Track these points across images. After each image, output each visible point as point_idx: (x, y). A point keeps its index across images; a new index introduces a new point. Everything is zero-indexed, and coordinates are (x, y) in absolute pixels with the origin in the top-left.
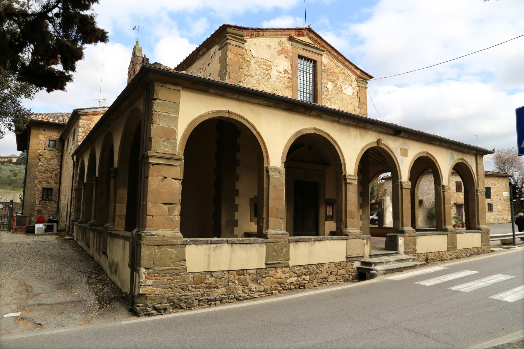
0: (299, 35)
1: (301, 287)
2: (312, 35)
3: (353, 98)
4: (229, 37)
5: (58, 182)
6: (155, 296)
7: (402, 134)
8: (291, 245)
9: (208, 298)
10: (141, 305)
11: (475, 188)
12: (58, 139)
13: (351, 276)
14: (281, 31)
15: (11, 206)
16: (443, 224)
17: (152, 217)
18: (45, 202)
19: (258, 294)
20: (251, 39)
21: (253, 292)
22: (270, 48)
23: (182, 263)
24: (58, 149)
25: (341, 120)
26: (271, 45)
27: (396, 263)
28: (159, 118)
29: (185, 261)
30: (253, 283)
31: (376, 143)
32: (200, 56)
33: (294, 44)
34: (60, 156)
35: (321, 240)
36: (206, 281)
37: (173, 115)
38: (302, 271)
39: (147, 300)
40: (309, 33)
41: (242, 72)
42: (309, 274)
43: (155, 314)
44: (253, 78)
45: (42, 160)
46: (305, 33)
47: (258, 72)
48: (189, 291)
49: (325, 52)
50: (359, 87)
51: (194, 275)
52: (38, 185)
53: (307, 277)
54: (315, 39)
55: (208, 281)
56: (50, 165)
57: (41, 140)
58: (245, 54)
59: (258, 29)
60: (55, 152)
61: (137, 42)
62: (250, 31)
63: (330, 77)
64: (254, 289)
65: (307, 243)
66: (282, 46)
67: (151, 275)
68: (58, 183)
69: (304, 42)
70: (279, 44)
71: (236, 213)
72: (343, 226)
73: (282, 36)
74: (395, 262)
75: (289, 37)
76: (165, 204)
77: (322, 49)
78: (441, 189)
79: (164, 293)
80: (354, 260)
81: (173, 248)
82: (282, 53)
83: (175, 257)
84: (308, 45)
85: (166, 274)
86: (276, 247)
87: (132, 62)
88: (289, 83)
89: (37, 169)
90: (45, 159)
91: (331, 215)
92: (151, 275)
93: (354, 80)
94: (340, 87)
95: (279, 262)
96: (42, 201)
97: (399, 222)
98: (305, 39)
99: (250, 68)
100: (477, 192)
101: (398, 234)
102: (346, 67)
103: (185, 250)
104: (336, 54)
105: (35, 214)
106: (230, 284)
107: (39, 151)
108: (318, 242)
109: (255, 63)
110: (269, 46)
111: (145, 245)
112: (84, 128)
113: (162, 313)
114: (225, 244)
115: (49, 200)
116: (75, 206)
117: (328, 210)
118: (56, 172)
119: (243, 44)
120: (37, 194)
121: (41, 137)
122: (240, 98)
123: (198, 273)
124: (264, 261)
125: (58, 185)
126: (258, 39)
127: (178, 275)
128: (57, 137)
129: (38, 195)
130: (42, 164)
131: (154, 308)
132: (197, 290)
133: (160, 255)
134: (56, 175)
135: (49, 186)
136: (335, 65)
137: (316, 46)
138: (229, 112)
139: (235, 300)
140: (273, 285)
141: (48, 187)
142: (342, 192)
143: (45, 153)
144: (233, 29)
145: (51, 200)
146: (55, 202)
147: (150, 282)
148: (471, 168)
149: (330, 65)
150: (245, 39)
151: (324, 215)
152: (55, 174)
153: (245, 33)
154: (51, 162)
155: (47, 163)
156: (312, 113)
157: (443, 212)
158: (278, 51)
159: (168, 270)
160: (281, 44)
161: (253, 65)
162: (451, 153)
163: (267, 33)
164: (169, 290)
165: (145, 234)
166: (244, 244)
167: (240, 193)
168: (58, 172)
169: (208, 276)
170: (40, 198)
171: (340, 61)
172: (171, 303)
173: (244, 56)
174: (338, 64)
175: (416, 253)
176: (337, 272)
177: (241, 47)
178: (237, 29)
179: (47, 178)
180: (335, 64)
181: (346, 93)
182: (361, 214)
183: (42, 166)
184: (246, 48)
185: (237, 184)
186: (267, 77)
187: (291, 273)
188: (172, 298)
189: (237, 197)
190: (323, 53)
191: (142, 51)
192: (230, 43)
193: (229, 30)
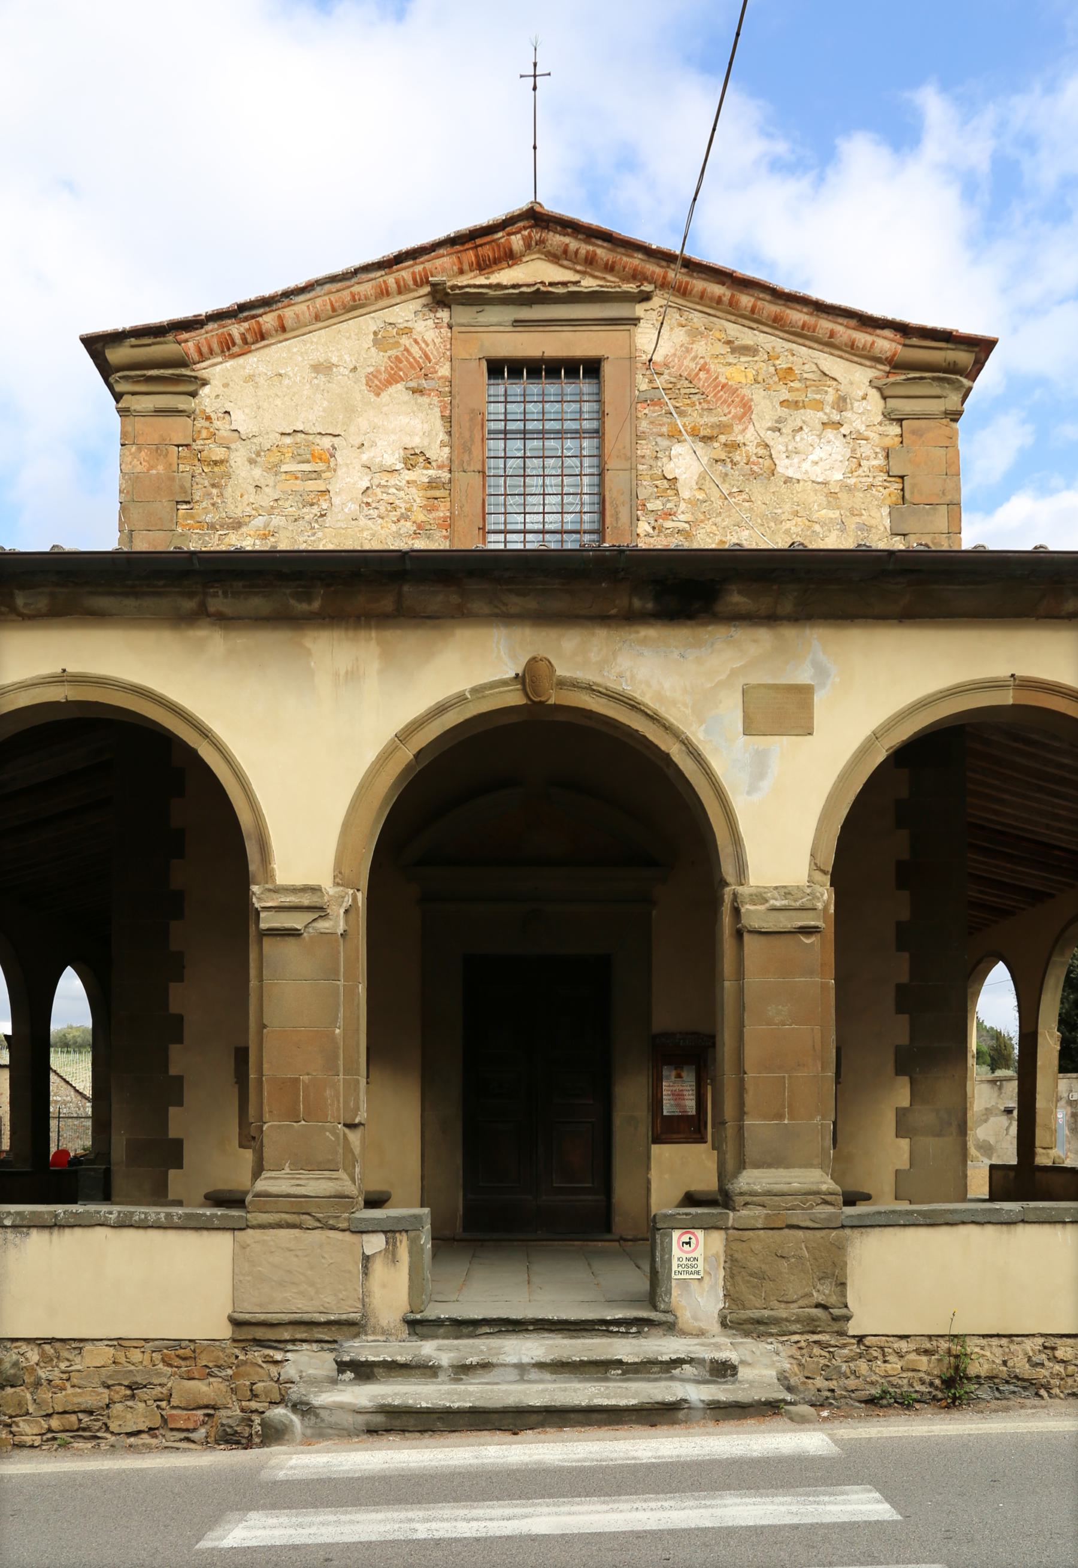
0: (483, 266)
2: (556, 240)
3: (849, 489)
14: (372, 275)
20: (230, 364)
26: (334, 360)
27: (548, 1376)
40: (536, 235)
41: (192, 517)
44: (244, 529)
46: (517, 242)
47: (265, 500)
49: (657, 301)
50: (900, 421)
54: (583, 252)
58: (204, 434)
59: (242, 307)
62: (210, 326)
69: (514, 286)
71: (173, 1111)
73: (393, 301)
74: (534, 1374)
77: (630, 287)
82: (393, 379)
84: (539, 296)
88: (430, 509)
91: (692, 1112)
94: (762, 451)
99: (228, 492)
102: (802, 335)
104: (717, 290)
109: (252, 462)
117: (667, 1087)
119: (193, 394)
126: (266, 350)
137: (589, 284)
142: (248, 981)
144: (133, 346)
149: (694, 358)
151: (643, 1114)
153: (190, 343)
158: (370, 379)
161: (243, 474)
163: (300, 308)
167: (189, 1031)
171: (752, 318)
174: (747, 336)
175: (842, 1333)
181: (798, 476)
182: (905, 1103)
184: (208, 410)
185: (175, 990)
186: (315, 510)
189: (178, 1046)
190: (639, 310)
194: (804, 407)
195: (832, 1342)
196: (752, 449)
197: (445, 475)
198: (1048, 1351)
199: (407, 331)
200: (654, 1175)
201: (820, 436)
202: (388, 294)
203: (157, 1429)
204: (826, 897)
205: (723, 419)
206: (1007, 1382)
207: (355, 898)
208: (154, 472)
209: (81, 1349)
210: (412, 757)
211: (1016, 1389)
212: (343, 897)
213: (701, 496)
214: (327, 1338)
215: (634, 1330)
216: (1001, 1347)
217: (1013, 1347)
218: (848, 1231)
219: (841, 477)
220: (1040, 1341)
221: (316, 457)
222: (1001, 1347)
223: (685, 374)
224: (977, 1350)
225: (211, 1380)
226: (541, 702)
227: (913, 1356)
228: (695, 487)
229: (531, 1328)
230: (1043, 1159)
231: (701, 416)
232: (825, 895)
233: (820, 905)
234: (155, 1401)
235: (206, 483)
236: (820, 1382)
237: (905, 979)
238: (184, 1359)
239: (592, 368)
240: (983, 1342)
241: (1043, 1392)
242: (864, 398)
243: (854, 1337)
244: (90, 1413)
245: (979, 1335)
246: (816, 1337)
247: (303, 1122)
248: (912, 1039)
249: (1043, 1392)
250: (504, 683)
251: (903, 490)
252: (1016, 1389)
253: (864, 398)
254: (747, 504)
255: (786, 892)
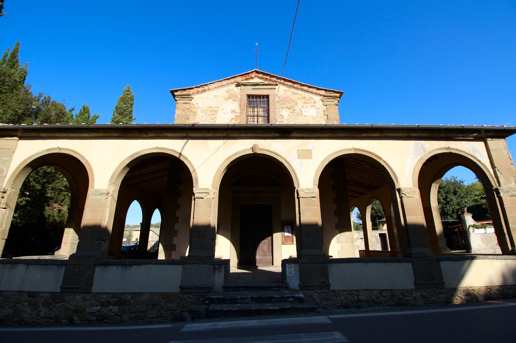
1: (101, 319)
8: (98, 270)
19: (45, 320)
26: (219, 95)
38: (109, 300)
40: (257, 74)
58: (192, 107)
64: (42, 314)
65: (120, 267)
69: (252, 83)
73: (230, 85)
77: (274, 83)
80: (194, 291)
82: (229, 98)
84: (257, 85)
94: (300, 111)
114: (21, 265)
137: (266, 83)
166: (41, 265)
186: (214, 121)
190: (276, 87)
194: (308, 103)
195: (327, 292)
196: (298, 110)
197: (239, 115)
198: (380, 294)
199: (233, 90)
200: (283, 252)
201: (311, 108)
202: (229, 84)
203: (159, 316)
204: (317, 190)
205: (292, 105)
206: (371, 302)
207: (216, 191)
208: (182, 114)
209: (142, 295)
210: (229, 163)
211: (374, 304)
212: (213, 191)
213: (288, 119)
214: (203, 292)
215: (278, 289)
216: (368, 293)
217: (371, 293)
218: (328, 264)
219: (315, 115)
220: (378, 291)
221: (215, 111)
222: (368, 293)
223: (285, 98)
224: (363, 294)
225: (174, 303)
226: (256, 153)
227: (347, 295)
228: (287, 117)
229: (253, 288)
230: (371, 249)
231: (288, 105)
232: (317, 191)
233: (316, 192)
234: (159, 309)
235: (192, 116)
236: (324, 302)
237: (336, 209)
238: (168, 298)
239: (267, 97)
240: (364, 292)
241: (380, 304)
242: (319, 102)
243: (332, 290)
244: (142, 312)
245: (363, 290)
246: (322, 291)
247: (201, 239)
249: (380, 304)
250: (249, 149)
251: (328, 117)
252: (374, 304)
253: (319, 102)
254: (297, 120)
255: (308, 189)
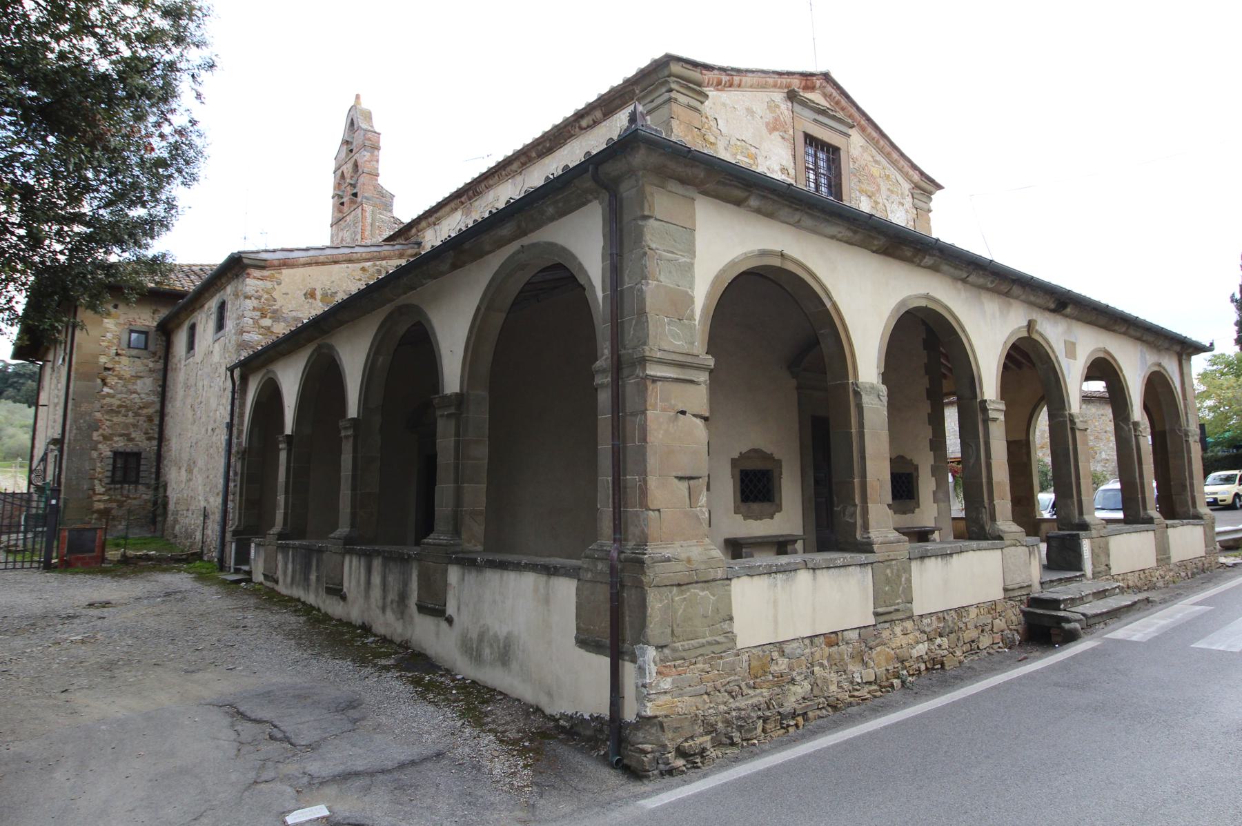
2: (830, 89)
4: (674, 86)
5: (156, 436)
6: (680, 720)
7: (1068, 310)
8: (915, 566)
9: (781, 710)
10: (648, 747)
11: (1181, 426)
12: (154, 329)
13: (1016, 634)
15: (54, 502)
16: (1141, 508)
17: (657, 513)
18: (122, 488)
21: (858, 687)
22: (753, 116)
23: (726, 626)
24: (154, 354)
25: (972, 279)
26: (754, 109)
28: (658, 264)
29: (731, 619)
30: (855, 662)
31: (1026, 329)
32: (581, 129)
33: (797, 108)
34: (159, 370)
35: (961, 552)
36: (773, 668)
37: (684, 259)
39: (664, 731)
40: (825, 84)
42: (947, 632)
43: (684, 768)
45: (112, 381)
46: (818, 83)
48: (743, 696)
51: (750, 654)
52: (100, 446)
53: (944, 642)
55: (776, 668)
56: (134, 393)
57: (107, 330)
59: (733, 69)
60: (145, 361)
61: (358, 97)
63: (865, 187)
65: (939, 559)
66: (775, 112)
67: (668, 664)
68: (154, 438)
69: (817, 104)
70: (769, 107)
72: (985, 517)
75: (787, 93)
76: (680, 478)
77: (850, 121)
78: (1130, 429)
79: (695, 708)
81: (708, 589)
82: (775, 129)
83: (712, 611)
84: (823, 112)
85: (697, 657)
86: (888, 571)
87: (346, 142)
89: (97, 405)
90: (120, 379)
92: (668, 664)
93: (907, 192)
95: (896, 607)
96: (112, 486)
97: (1074, 504)
98: (816, 97)
100: (1187, 435)
101: (1081, 533)
102: (894, 163)
103: (730, 591)
104: (874, 134)
105: (93, 521)
106: (816, 669)
107: (103, 359)
108: (918, 562)
109: (726, 149)
110: (750, 111)
111: (654, 586)
112: (259, 298)
113: (697, 763)
114: (802, 571)
115: (130, 483)
116: (241, 495)
118: (150, 411)
120: (98, 470)
121: (109, 323)
122: (802, 223)
123: (756, 649)
124: (872, 609)
125: (155, 443)
126: (728, 93)
127: (721, 658)
128: (150, 324)
129: (102, 469)
130: (111, 391)
131: (681, 753)
132: (758, 691)
133: (684, 611)
134: (150, 419)
135: (130, 447)
136: (871, 159)
137: (840, 115)
138: (782, 255)
139: (829, 709)
140: (889, 665)
141: (128, 450)
143: (119, 362)
144: (682, 66)
145: (137, 482)
146: (148, 486)
147: (666, 684)
148: (1173, 382)
150: (707, 93)
152: (148, 417)
153: (708, 76)
154: (135, 387)
155: (124, 389)
156: (925, 260)
157: (1138, 480)
158: (767, 124)
159: (703, 646)
160: (772, 106)
162: (1141, 351)
163: (747, 80)
164: (704, 700)
165: (653, 558)
168: (154, 410)
169: (775, 655)
170: (107, 477)
171: (881, 150)
172: (711, 732)
173: (703, 131)
174: (879, 158)
176: (992, 625)
177: (697, 110)
178: (691, 68)
179: (126, 426)
180: (873, 157)
183: (112, 396)
187: (917, 633)
188: (712, 720)
190: (850, 131)
191: (371, 118)
192: (676, 100)
193: (675, 68)
248: (935, 462)
